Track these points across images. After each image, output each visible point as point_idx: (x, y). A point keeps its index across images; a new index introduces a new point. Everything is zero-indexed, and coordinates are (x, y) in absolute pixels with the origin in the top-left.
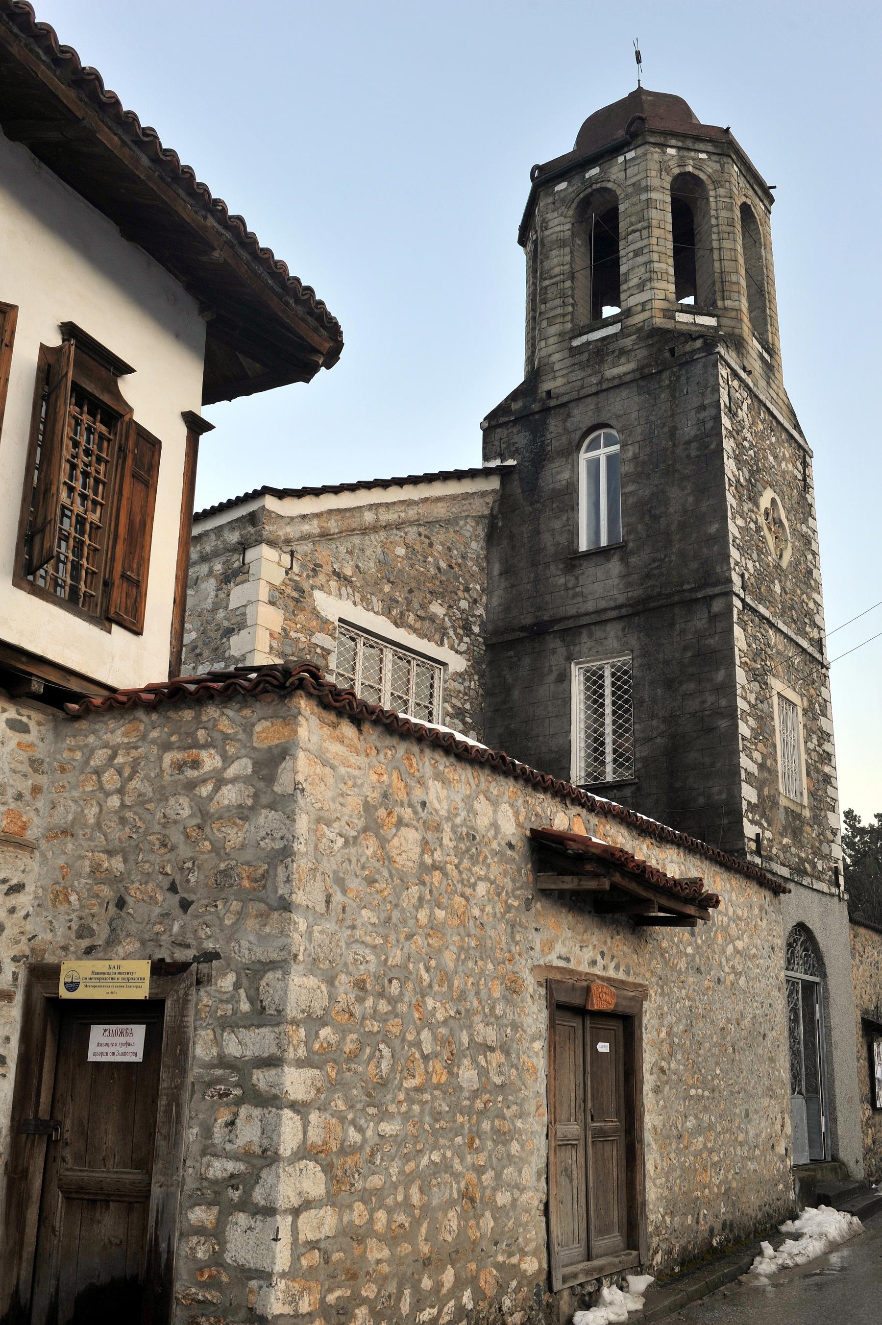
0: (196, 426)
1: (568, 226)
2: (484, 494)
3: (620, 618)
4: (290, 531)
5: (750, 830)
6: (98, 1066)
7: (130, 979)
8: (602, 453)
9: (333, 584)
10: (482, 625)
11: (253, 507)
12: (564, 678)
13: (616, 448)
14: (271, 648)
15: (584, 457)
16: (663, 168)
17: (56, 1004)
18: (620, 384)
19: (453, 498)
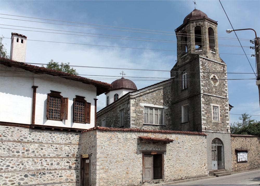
0: (96, 100)
1: (180, 38)
2: (170, 83)
3: (187, 99)
4: (135, 96)
5: (203, 127)
6: (87, 163)
7: (87, 156)
8: (186, 74)
9: (143, 102)
10: (171, 102)
11: (129, 95)
12: (181, 108)
13: (187, 73)
14: (133, 112)
15: (183, 75)
16: (193, 26)
17: (82, 158)
18: (187, 63)
19: (164, 85)
